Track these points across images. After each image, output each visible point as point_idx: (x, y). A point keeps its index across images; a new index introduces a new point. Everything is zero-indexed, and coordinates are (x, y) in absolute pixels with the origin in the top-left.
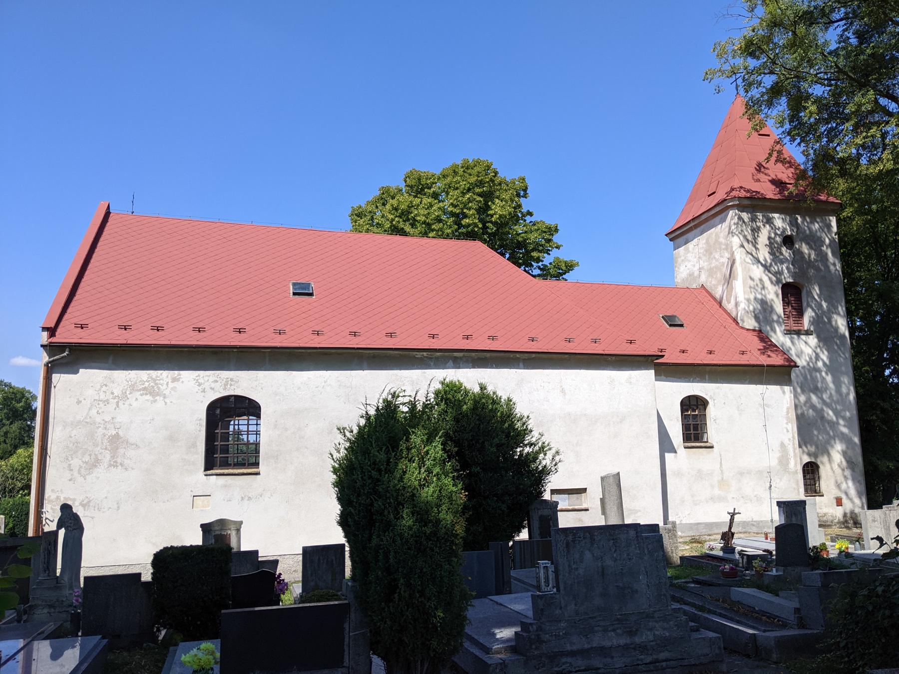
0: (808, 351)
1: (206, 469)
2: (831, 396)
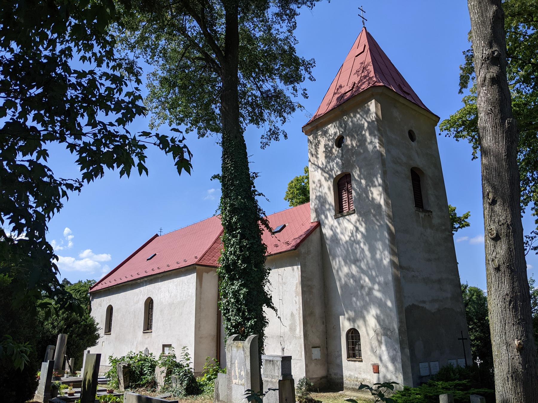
0: (350, 227)
1: (348, 358)
2: (368, 264)
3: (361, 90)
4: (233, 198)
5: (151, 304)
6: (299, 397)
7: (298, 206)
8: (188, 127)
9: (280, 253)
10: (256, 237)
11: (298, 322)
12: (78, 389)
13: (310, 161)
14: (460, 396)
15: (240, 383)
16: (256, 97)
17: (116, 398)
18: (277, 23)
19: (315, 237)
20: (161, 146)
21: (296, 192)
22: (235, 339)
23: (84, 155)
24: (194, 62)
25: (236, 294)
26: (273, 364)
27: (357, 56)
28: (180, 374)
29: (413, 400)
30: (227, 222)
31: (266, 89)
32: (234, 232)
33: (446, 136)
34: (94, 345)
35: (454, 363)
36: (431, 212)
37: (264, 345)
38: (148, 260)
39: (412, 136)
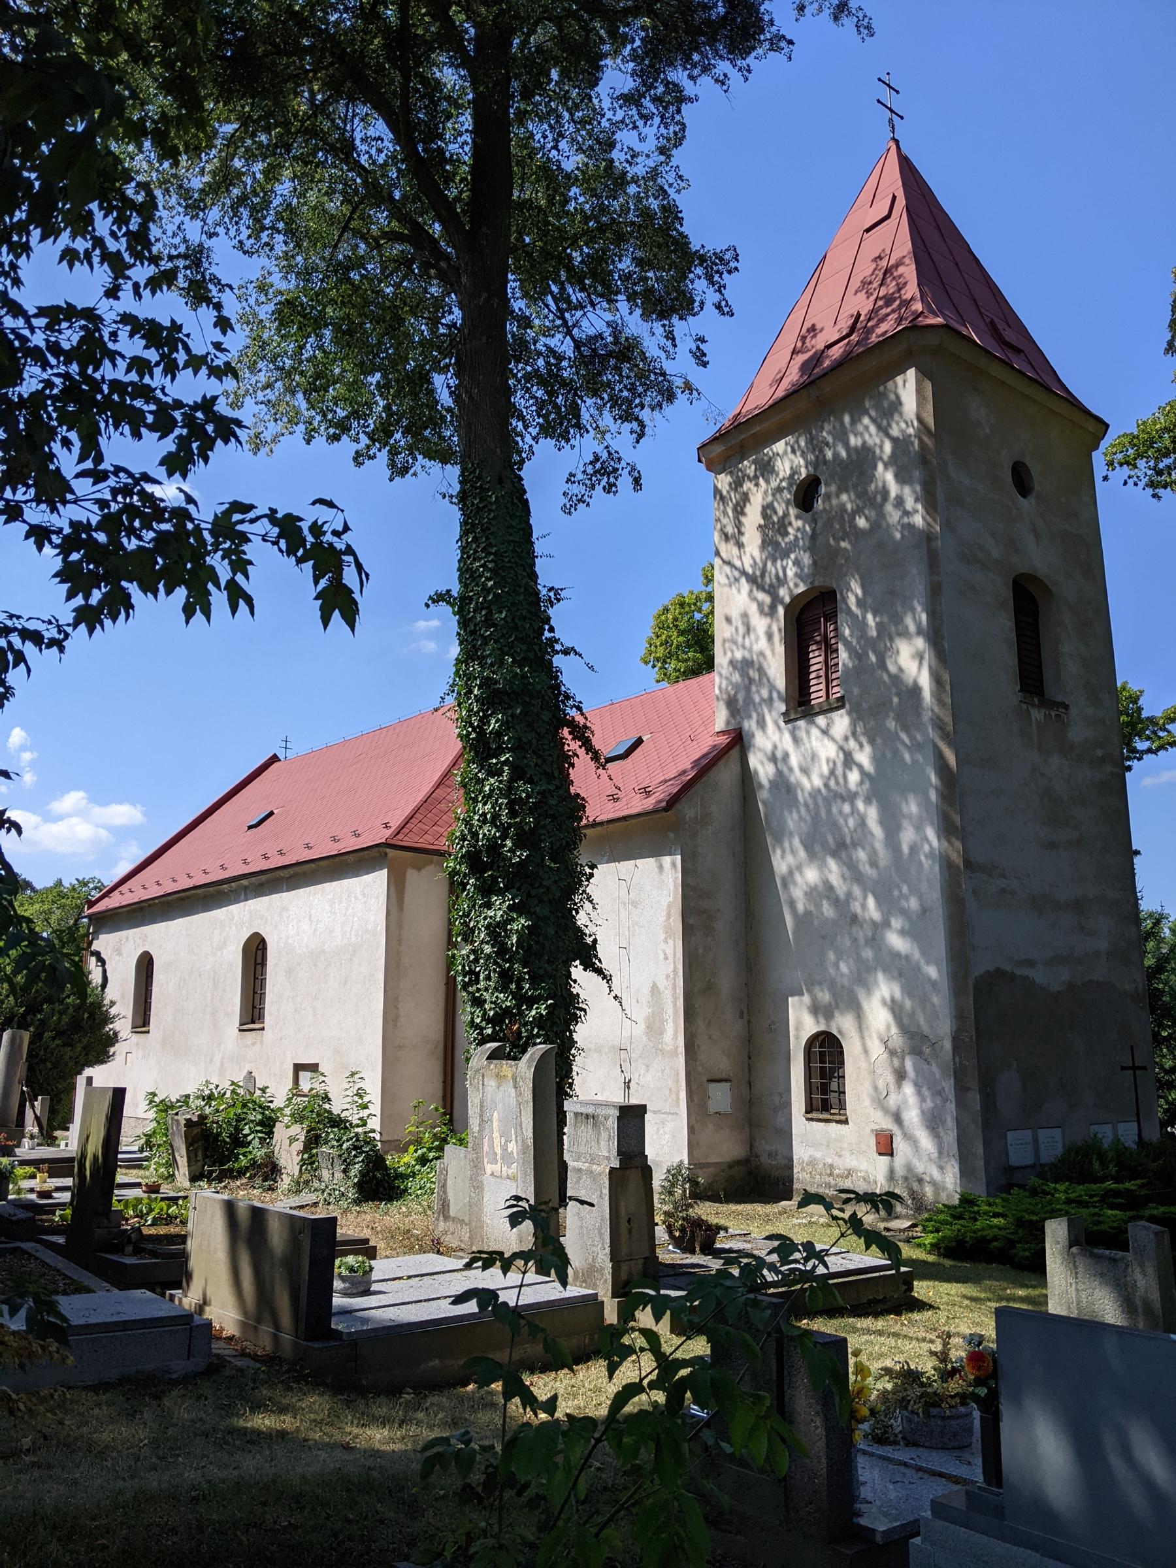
0: (827, 751)
1: (807, 1112)
3: (874, 339)
4: (489, 661)
5: (260, 952)
6: (665, 1213)
7: (681, 684)
8: (361, 446)
9: (625, 818)
10: (556, 773)
11: (669, 1010)
12: (62, 1179)
13: (717, 553)
14: (1115, 1225)
15: (504, 1174)
16: (560, 358)
17: (169, 1207)
18: (627, 125)
19: (726, 775)
20: (283, 544)
21: (677, 639)
22: (493, 1056)
23: (75, 557)
24: (378, 246)
25: (496, 932)
26: (595, 1125)
27: (868, 230)
28: (341, 1146)
29: (983, 1229)
30: (474, 730)
31: (592, 332)
32: (494, 761)
33: (1125, 483)
34: (102, 1062)
35: (1105, 1133)
36: (1067, 707)
37: (574, 1073)
38: (250, 827)
39: (1022, 480)
